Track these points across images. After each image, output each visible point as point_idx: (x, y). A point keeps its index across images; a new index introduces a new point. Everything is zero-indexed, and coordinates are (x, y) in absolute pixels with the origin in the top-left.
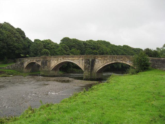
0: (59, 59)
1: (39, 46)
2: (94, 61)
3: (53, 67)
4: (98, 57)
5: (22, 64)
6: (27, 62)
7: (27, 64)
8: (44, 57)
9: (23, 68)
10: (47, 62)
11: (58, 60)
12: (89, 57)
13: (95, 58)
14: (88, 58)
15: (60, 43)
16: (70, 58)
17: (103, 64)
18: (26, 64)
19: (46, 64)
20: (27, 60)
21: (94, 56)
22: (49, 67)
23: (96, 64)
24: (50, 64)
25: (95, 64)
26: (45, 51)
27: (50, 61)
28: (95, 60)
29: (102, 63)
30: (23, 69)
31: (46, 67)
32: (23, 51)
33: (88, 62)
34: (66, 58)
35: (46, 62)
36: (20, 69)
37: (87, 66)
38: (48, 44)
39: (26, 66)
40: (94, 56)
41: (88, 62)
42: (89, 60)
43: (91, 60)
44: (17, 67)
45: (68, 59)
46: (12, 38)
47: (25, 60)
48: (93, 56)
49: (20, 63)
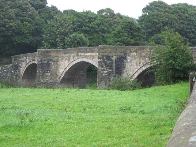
0: (70, 56)
1: (62, 25)
2: (122, 60)
3: (63, 75)
4: (131, 52)
5: (17, 67)
6: (25, 64)
7: (26, 68)
8: (44, 52)
9: (18, 76)
10: (50, 64)
11: (69, 60)
12: (109, 50)
13: (125, 54)
14: (107, 54)
15: (142, 19)
16: (87, 54)
17: (139, 67)
18: (23, 69)
19: (49, 69)
20: (25, 58)
21: (123, 47)
22: (56, 74)
23: (128, 66)
24: (57, 67)
25: (124, 67)
26: (75, 39)
27: (56, 61)
28: (125, 58)
29: (137, 64)
30: (17, 80)
31: (49, 74)
32: (32, 39)
33: (109, 62)
34: (82, 54)
35: (48, 64)
36: (12, 78)
37: (106, 72)
38: (90, 22)
39: (24, 72)
40: (123, 47)
41: (109, 62)
42: (109, 58)
43: (114, 58)
44: (6, 76)
45: (86, 57)
46: (7, 9)
47: (22, 59)
48: (120, 48)
49: (12, 67)
